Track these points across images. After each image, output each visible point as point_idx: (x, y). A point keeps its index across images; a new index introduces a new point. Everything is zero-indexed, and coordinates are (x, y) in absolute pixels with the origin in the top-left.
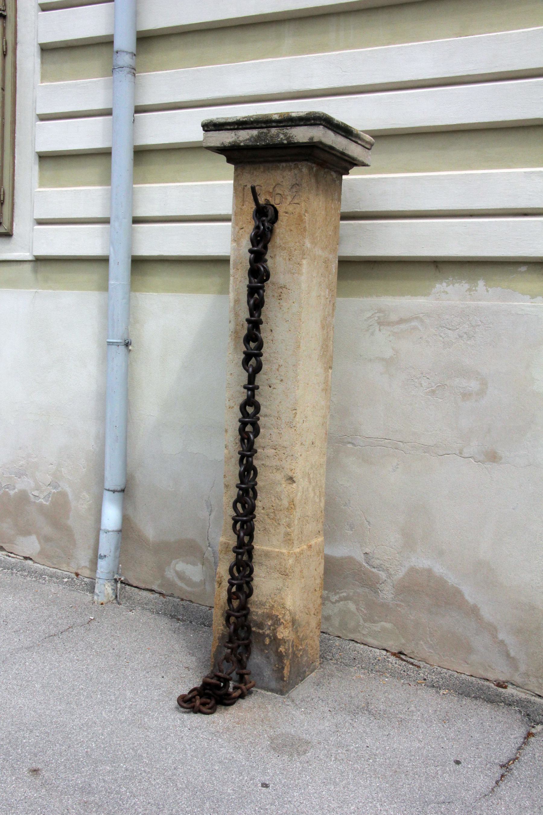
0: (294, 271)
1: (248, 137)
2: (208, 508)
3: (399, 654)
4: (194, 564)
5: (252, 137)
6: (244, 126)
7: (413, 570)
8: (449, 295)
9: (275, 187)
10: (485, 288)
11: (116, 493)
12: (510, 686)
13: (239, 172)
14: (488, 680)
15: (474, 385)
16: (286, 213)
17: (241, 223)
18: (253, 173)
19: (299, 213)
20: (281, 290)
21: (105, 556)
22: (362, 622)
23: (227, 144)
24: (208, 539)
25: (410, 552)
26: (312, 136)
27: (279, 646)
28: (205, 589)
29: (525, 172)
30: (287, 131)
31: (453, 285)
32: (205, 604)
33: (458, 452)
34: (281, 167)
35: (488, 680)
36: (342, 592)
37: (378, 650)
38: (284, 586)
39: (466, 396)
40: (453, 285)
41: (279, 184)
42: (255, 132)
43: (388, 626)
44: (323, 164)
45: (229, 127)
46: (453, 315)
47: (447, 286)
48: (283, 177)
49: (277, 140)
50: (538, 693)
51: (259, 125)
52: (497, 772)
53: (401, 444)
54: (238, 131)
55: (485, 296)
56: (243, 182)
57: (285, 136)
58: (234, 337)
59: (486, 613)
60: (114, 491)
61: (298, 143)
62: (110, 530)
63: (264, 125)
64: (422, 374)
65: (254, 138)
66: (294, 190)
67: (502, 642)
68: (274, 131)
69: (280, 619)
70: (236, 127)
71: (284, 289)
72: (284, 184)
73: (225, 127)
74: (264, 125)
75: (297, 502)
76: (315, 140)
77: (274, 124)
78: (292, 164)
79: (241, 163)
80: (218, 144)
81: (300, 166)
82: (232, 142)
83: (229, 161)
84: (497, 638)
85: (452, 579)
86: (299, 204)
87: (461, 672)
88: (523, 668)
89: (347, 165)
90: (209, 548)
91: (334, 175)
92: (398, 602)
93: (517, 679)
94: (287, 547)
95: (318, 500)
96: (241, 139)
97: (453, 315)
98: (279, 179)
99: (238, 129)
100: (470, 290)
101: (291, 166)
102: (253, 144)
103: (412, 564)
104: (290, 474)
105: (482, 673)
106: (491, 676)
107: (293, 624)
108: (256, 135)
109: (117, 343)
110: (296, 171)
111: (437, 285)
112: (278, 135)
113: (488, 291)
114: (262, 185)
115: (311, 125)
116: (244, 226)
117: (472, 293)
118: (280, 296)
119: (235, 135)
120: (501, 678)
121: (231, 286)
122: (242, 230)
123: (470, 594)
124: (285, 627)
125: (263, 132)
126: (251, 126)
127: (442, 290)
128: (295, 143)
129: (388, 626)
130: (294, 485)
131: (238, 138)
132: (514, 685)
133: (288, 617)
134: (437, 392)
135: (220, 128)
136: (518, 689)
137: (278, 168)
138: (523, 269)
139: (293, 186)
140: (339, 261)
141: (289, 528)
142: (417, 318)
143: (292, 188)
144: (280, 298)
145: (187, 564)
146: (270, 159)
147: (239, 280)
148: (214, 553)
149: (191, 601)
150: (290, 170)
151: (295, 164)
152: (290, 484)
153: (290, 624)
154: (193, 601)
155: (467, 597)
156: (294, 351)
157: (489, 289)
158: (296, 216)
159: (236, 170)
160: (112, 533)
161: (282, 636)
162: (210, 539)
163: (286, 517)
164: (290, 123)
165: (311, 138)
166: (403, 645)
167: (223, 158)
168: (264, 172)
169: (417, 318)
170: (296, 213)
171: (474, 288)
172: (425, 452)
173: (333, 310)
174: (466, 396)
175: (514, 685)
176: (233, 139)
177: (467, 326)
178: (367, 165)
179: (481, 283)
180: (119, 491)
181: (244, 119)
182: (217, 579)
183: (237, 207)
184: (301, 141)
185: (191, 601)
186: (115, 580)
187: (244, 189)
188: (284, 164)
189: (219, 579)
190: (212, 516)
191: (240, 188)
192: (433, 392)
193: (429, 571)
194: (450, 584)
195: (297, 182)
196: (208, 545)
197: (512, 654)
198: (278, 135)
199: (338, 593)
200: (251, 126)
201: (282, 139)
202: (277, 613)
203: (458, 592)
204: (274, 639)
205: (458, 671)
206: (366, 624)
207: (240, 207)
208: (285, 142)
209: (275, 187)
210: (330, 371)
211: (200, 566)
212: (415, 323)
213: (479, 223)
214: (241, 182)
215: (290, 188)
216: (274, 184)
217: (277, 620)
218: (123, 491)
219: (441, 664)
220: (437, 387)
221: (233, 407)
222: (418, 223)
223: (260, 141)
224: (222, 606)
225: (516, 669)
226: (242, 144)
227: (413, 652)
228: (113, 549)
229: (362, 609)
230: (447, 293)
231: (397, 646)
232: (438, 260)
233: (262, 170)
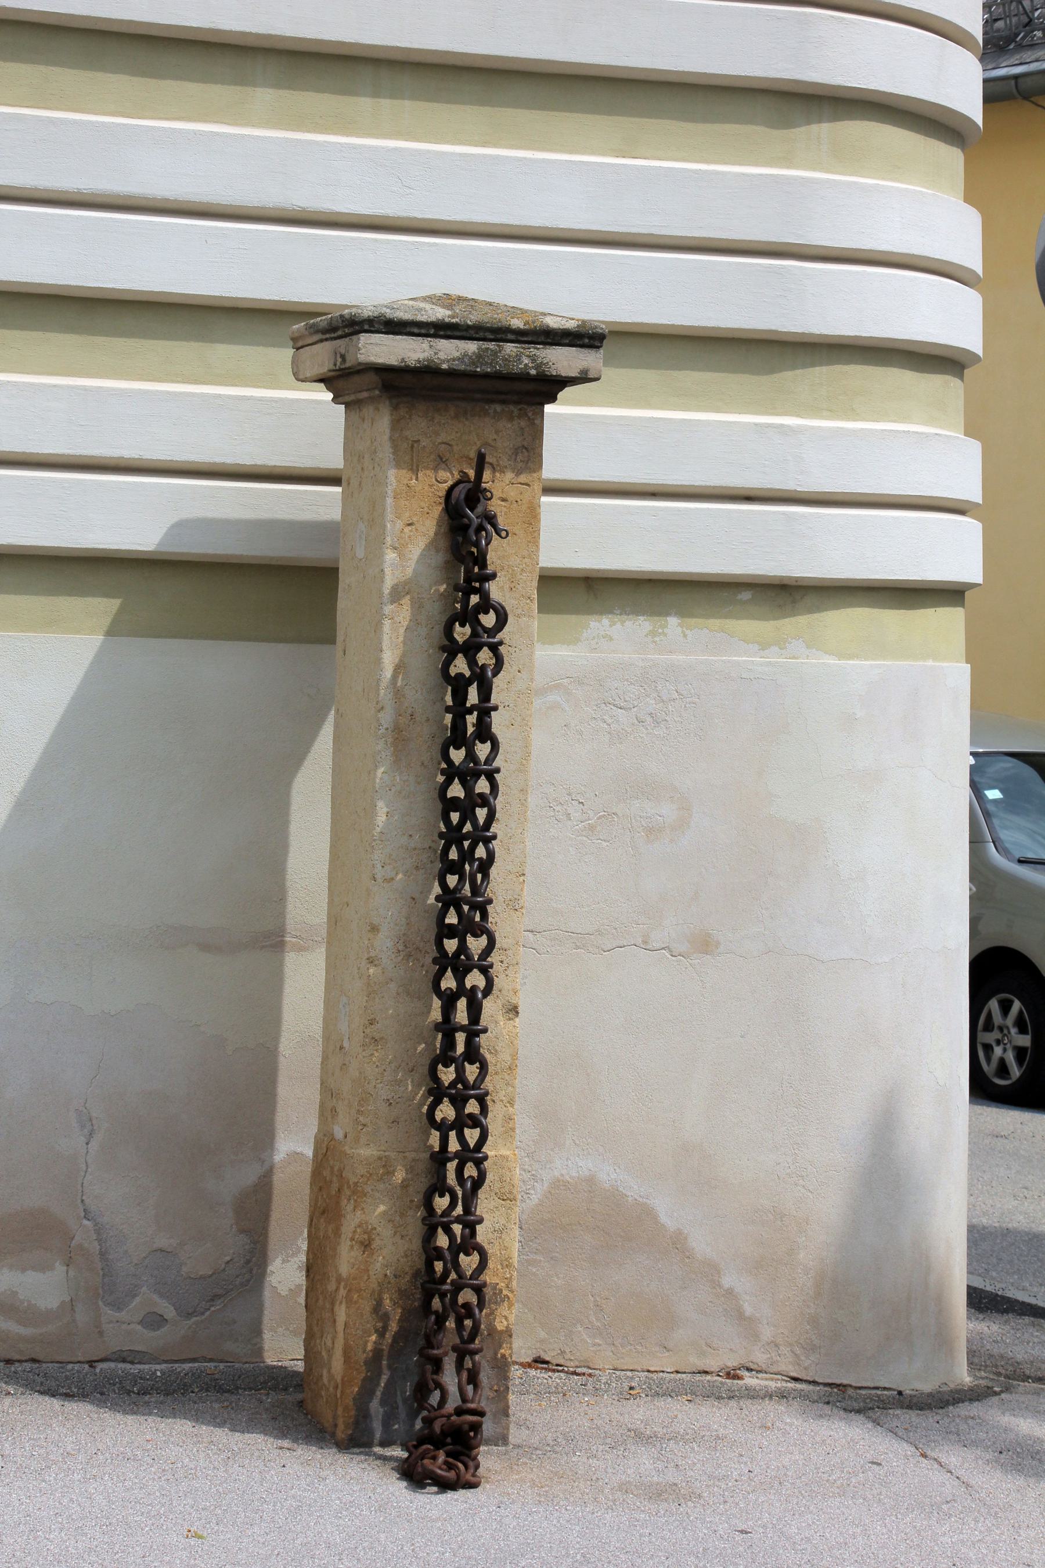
0: (519, 611)
1: (457, 354)
2: (83, 1127)
4: (43, 1267)
5: (465, 355)
6: (449, 333)
7: (558, 1184)
10: (679, 629)
12: (747, 1374)
13: (402, 411)
14: (706, 1372)
15: (668, 811)
16: (504, 500)
17: (407, 514)
18: (433, 418)
23: (412, 363)
24: (82, 1201)
25: (552, 1150)
27: (500, 1347)
28: (74, 1321)
29: (756, 424)
30: (538, 353)
31: (623, 623)
32: (76, 1359)
33: (639, 941)
34: (491, 411)
35: (706, 1372)
39: (652, 832)
40: (623, 623)
42: (472, 347)
45: (416, 330)
46: (627, 680)
47: (611, 626)
48: (497, 432)
50: (794, 1374)
51: (481, 335)
53: (530, 934)
54: (437, 340)
55: (681, 643)
57: (534, 361)
58: (390, 740)
59: (701, 1243)
64: (569, 794)
65: (470, 357)
66: (520, 457)
67: (730, 1292)
68: (510, 348)
69: (501, 1291)
70: (432, 331)
73: (408, 330)
77: (510, 336)
78: (514, 409)
81: (530, 414)
82: (424, 360)
84: (720, 1286)
85: (634, 1188)
86: (528, 485)
87: (657, 1369)
88: (767, 1333)
90: (85, 1222)
92: (532, 1256)
93: (760, 1358)
94: (508, 1144)
96: (442, 356)
97: (627, 680)
99: (435, 336)
100: (653, 633)
102: (468, 368)
103: (556, 1173)
105: (696, 1361)
106: (713, 1364)
108: (474, 353)
111: (592, 624)
113: (685, 636)
115: (582, 346)
116: (415, 519)
117: (657, 639)
119: (431, 347)
120: (729, 1364)
121: (386, 639)
122: (410, 528)
123: (669, 1211)
127: (603, 633)
131: (436, 354)
132: (752, 1370)
134: (599, 828)
135: (397, 330)
136: (760, 1375)
138: (746, 595)
139: (516, 451)
142: (557, 687)
145: (24, 1270)
148: (98, 1232)
149: (34, 1360)
150: (511, 419)
151: (520, 410)
152: (510, 1019)
154: (41, 1359)
155: (663, 1219)
156: (522, 764)
157: (688, 632)
158: (524, 507)
162: (87, 1201)
164: (542, 339)
166: (542, 1341)
168: (456, 417)
169: (557, 687)
171: (660, 631)
172: (577, 947)
174: (652, 832)
175: (752, 1370)
176: (426, 355)
177: (653, 702)
179: (673, 621)
181: (454, 321)
185: (34, 1360)
187: (412, 447)
188: (498, 408)
189: (366, 1236)
190: (94, 1145)
192: (592, 828)
193: (591, 1180)
194: (630, 1199)
195: (526, 444)
196: (83, 1214)
197: (748, 1310)
198: (518, 358)
200: (464, 333)
201: (526, 365)
202: (495, 1280)
203: (647, 1213)
204: (489, 1335)
205: (652, 1369)
208: (533, 372)
211: (60, 1269)
212: (553, 697)
213: (679, 510)
214: (407, 433)
217: (495, 1294)
219: (618, 1364)
220: (598, 818)
221: (392, 879)
222: (566, 505)
223: (482, 364)
224: (374, 1291)
225: (756, 1336)
226: (445, 366)
227: (563, 1352)
230: (611, 639)
231: (529, 1348)
232: (595, 575)
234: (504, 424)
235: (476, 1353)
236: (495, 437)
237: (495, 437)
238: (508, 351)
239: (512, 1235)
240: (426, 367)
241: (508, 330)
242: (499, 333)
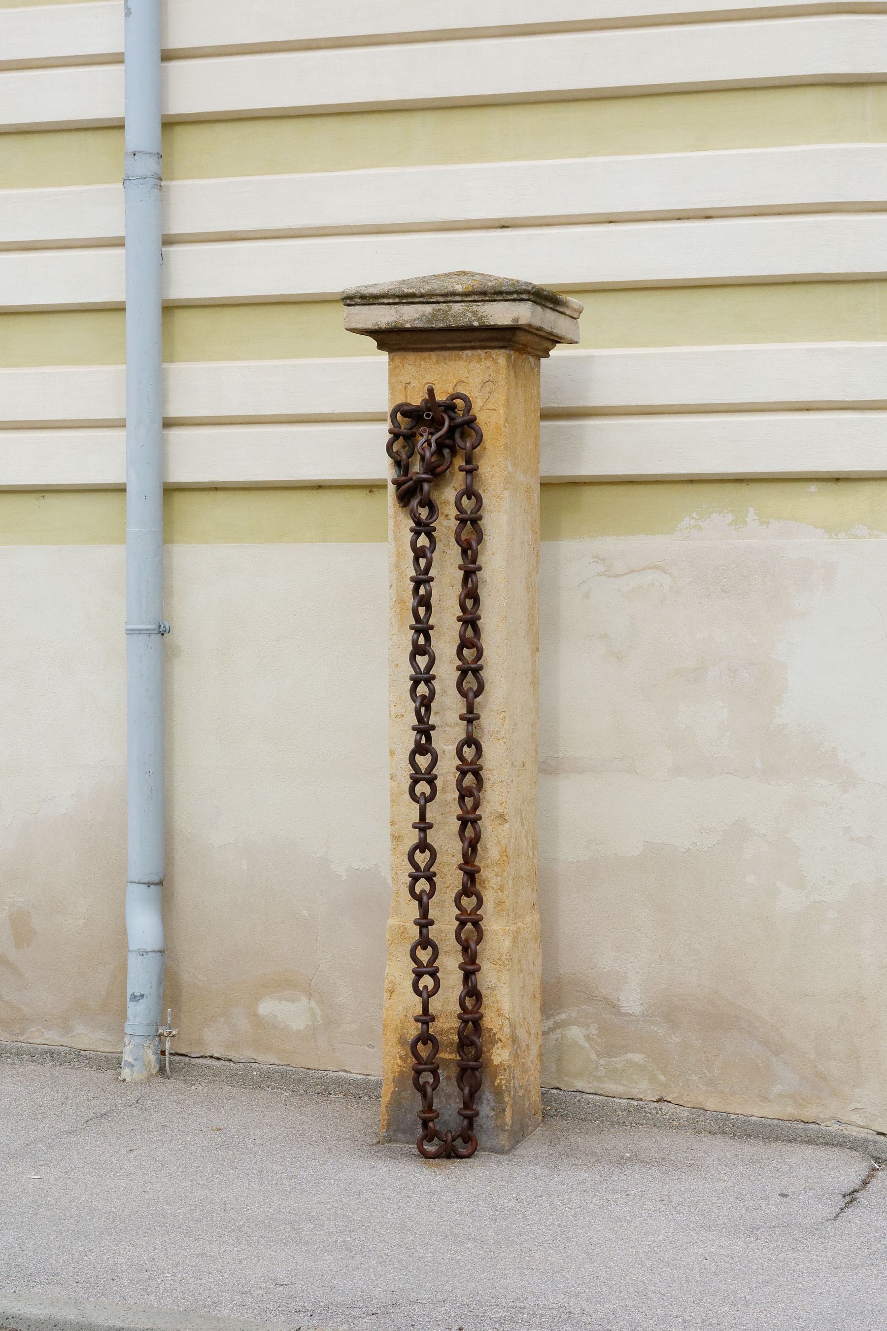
3: (660, 1100)
8: (710, 532)
11: (152, 887)
19: (497, 423)
21: (142, 996)
22: (594, 1056)
34: (464, 356)
36: (559, 1014)
37: (625, 1101)
38: (499, 981)
42: (428, 309)
43: (637, 1058)
44: (523, 350)
45: (386, 301)
49: (464, 322)
52: (842, 1202)
56: (405, 377)
60: (149, 884)
62: (149, 949)
63: (441, 299)
68: (457, 308)
72: (470, 380)
74: (441, 299)
75: (510, 852)
76: (521, 322)
77: (458, 298)
79: (399, 350)
80: (369, 326)
83: (381, 346)
89: (547, 344)
91: (532, 359)
95: (531, 854)
96: (406, 318)
101: (479, 355)
102: (426, 326)
104: (500, 810)
107: (514, 1042)
109: (147, 630)
110: (489, 363)
112: (463, 314)
114: (435, 382)
124: (503, 1047)
125: (439, 309)
126: (421, 299)
129: (637, 1058)
130: (507, 825)
133: (507, 1030)
140: (541, 484)
141: (502, 891)
146: (449, 345)
152: (500, 824)
153: (510, 1042)
159: (391, 360)
160: (151, 955)
161: (500, 1060)
163: (497, 875)
165: (517, 320)
167: (372, 343)
170: (492, 423)
173: (537, 562)
178: (576, 343)
180: (156, 884)
182: (386, 985)
186: (160, 1035)
187: (406, 388)
191: (401, 387)
199: (552, 1015)
200: (421, 299)
206: (602, 1061)
208: (476, 324)
210: (537, 655)
214: (401, 378)
216: (455, 382)
218: (160, 883)
226: (408, 326)
228: (155, 984)
229: (595, 1037)
233: (434, 361)
234: (474, 365)
235: (477, 1069)
236: (467, 375)
237: (467, 375)
238: (456, 310)
239: (503, 992)
240: (395, 327)
241: (454, 294)
242: (449, 297)
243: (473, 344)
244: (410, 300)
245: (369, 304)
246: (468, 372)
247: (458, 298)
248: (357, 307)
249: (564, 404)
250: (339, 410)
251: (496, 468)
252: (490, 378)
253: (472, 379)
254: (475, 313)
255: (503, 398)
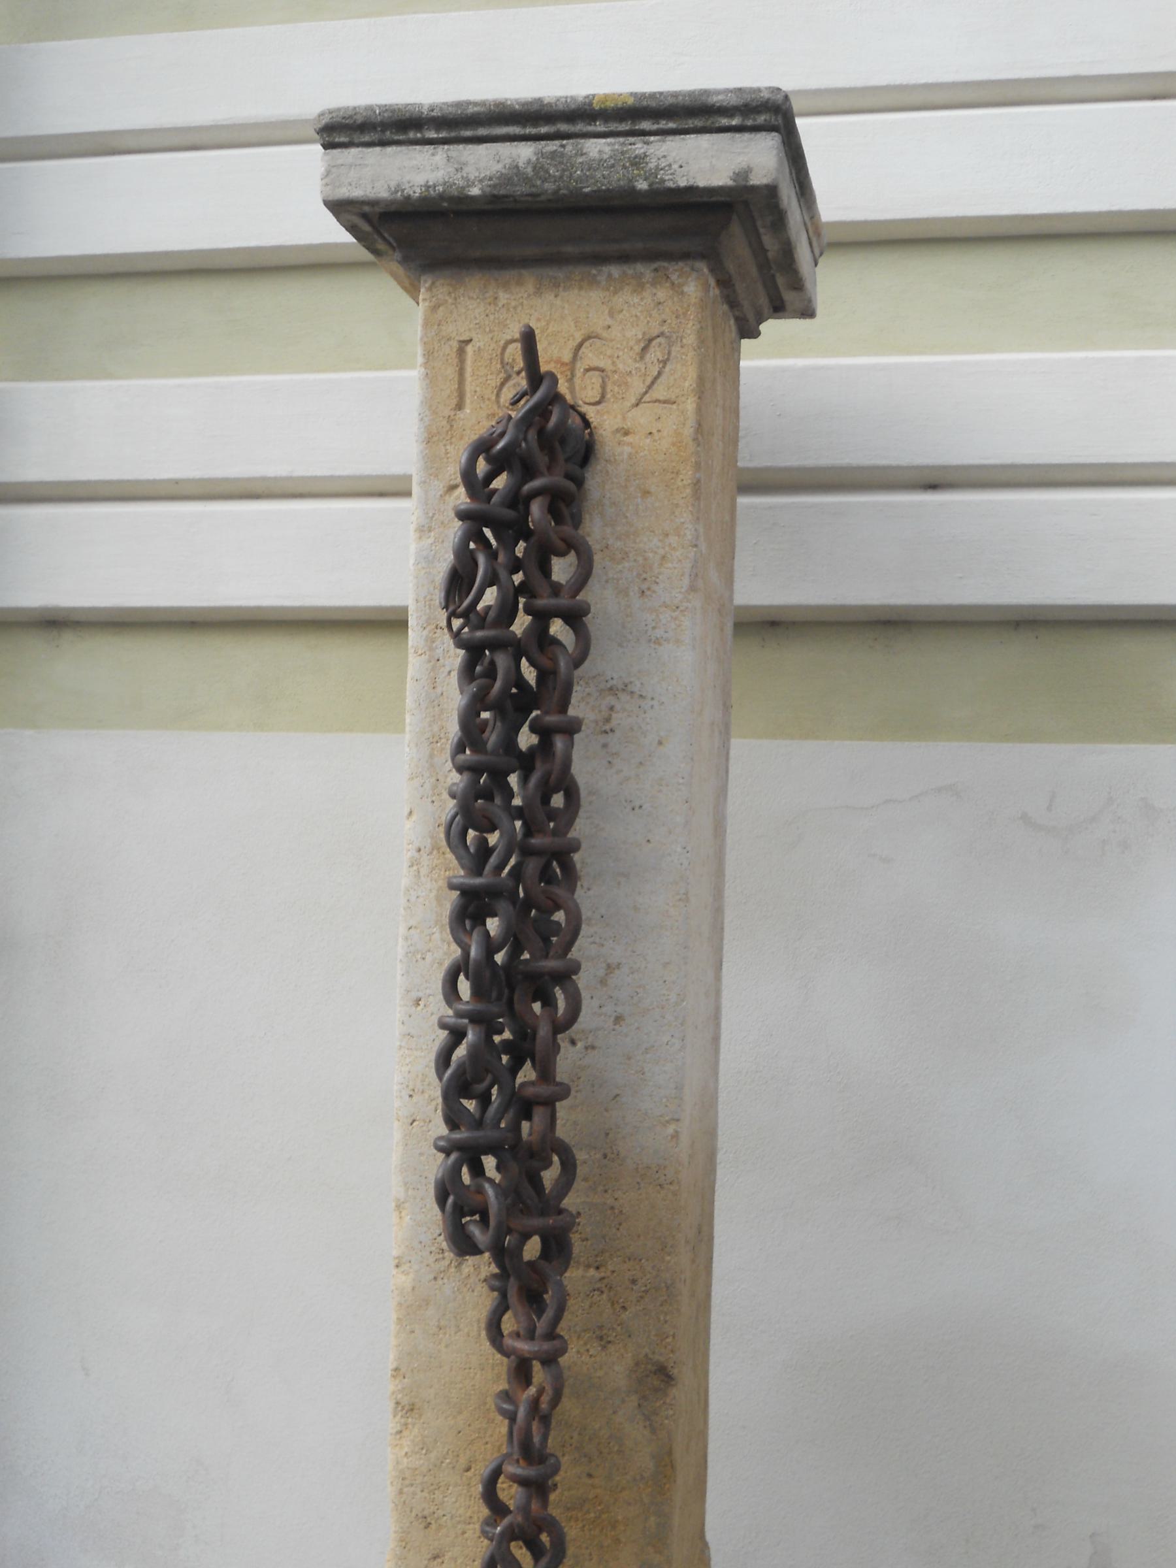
0: (659, 633)
9: (580, 345)
20: (610, 700)
26: (744, 165)
31: (395, 1532)
40: (395, 1532)
41: (597, 337)
42: (525, 153)
49: (616, 179)
61: (691, 190)
68: (596, 148)
71: (624, 697)
78: (645, 270)
81: (674, 277)
96: (472, 172)
98: (598, 319)
110: (662, 294)
118: (608, 720)
119: (449, 159)
128: (679, 191)
137: (593, 282)
143: (645, 349)
144: (607, 727)
147: (428, 679)
150: (640, 287)
165: (744, 174)
183: (435, 413)
184: (702, 183)
187: (461, 352)
188: (615, 270)
207: (447, 412)
208: (642, 185)
209: (580, 345)
214: (449, 329)
215: (638, 349)
226: (475, 191)
234: (626, 298)
236: (609, 321)
237: (609, 321)
243: (626, 246)
244: (482, 132)
245: (383, 144)
246: (611, 314)
247: (600, 127)
248: (354, 151)
249: (810, 461)
250: (301, 471)
251: (673, 540)
252: (665, 329)
253: (615, 340)
254: (638, 162)
255: (692, 373)
